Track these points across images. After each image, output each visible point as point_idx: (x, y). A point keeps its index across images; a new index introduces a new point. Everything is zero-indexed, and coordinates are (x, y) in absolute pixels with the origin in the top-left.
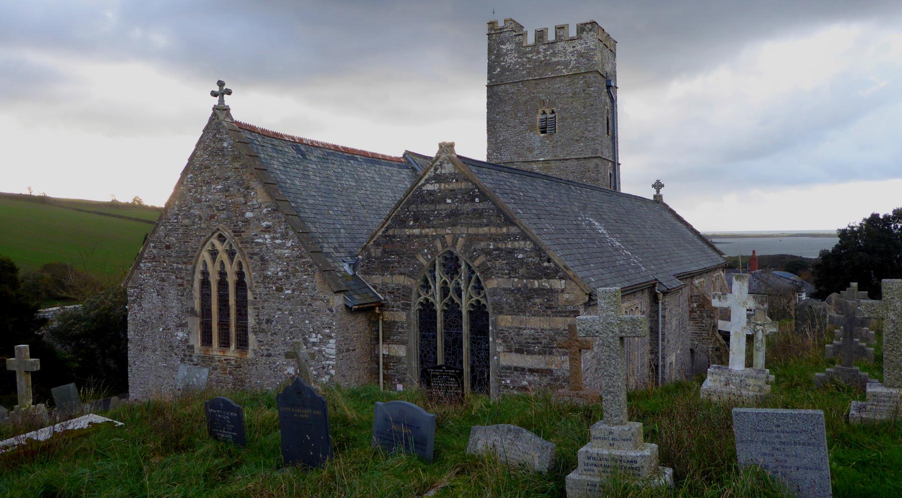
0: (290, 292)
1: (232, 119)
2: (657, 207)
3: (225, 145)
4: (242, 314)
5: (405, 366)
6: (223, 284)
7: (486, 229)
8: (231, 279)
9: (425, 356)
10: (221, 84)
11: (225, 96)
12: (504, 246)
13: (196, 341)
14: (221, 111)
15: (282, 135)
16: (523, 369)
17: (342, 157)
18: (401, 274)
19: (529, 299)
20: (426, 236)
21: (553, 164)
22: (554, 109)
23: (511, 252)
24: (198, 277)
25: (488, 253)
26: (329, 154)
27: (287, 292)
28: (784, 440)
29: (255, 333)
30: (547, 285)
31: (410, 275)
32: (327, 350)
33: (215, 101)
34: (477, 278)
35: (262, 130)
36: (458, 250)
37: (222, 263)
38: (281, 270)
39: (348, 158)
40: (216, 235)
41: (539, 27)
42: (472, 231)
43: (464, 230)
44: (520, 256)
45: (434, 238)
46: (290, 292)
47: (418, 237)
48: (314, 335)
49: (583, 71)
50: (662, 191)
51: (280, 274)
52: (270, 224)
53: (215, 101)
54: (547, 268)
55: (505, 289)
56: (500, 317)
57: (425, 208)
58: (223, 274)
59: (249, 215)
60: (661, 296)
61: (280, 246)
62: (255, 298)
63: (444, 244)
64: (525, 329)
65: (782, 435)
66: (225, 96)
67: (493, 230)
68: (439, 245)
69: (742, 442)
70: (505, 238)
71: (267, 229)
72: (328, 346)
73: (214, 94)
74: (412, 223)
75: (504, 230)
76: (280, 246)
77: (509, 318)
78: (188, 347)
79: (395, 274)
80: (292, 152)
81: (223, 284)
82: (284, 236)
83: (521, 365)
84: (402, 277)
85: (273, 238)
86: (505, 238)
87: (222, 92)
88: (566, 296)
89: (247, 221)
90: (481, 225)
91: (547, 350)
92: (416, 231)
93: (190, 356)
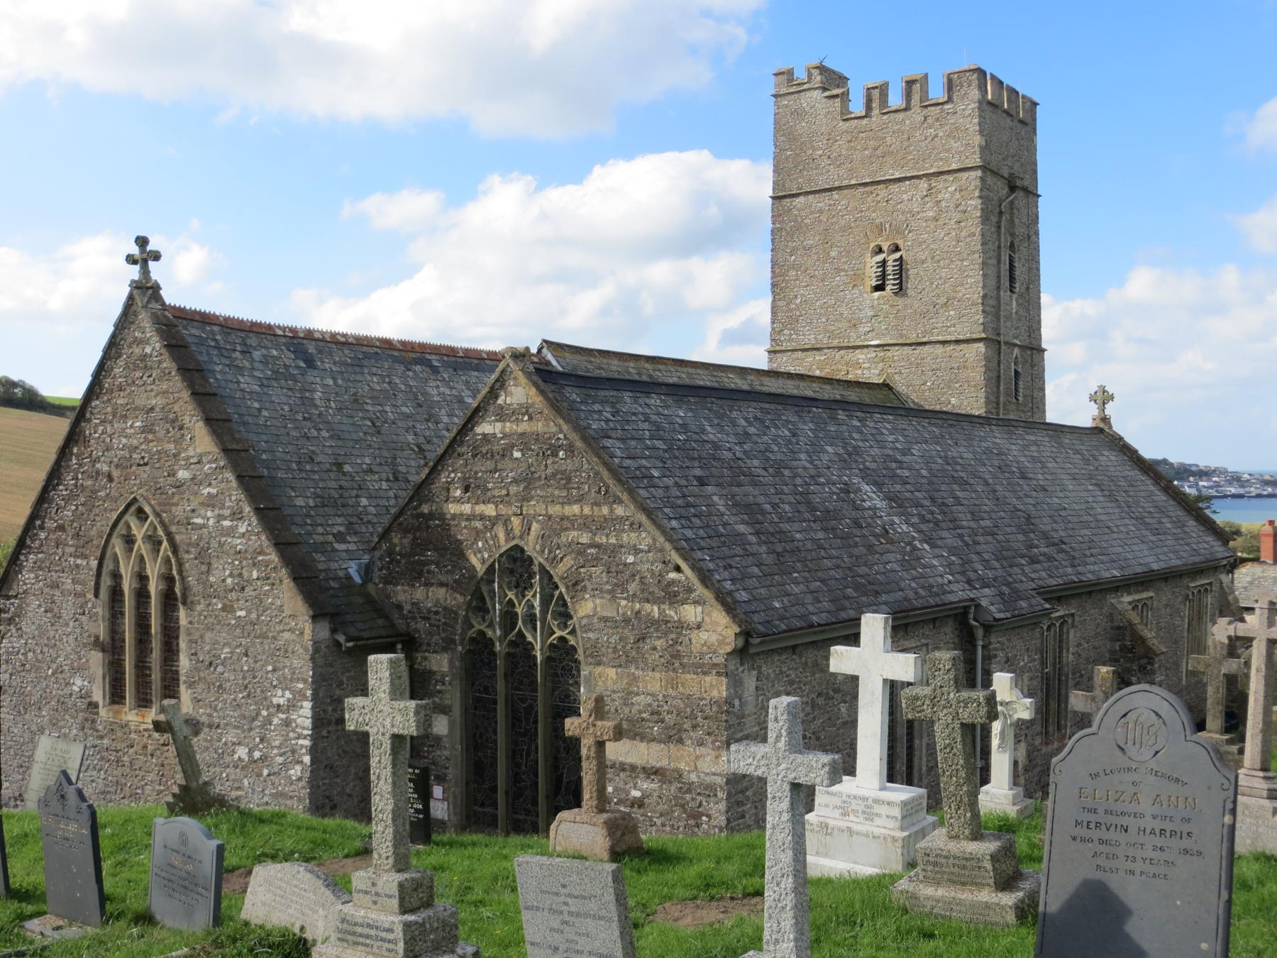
0: (243, 613)
1: (163, 304)
2: (1015, 448)
3: (148, 350)
4: (170, 651)
5: (446, 753)
6: (142, 595)
7: (576, 509)
8: (154, 587)
9: (481, 737)
10: (142, 242)
11: (151, 264)
12: (604, 540)
13: (98, 696)
14: (146, 290)
15: (269, 327)
16: (633, 768)
17: (396, 360)
18: (441, 584)
19: (642, 639)
20: (482, 517)
21: (895, 352)
22: (900, 242)
23: (615, 550)
24: (106, 581)
25: (580, 550)
26: (367, 356)
27: (239, 613)
28: (573, 909)
29: (191, 685)
30: (672, 613)
31: (456, 587)
32: (299, 721)
33: (134, 272)
34: (561, 596)
35: (227, 319)
36: (531, 546)
37: (142, 559)
38: (231, 575)
39: (408, 364)
40: (133, 509)
41: (914, 72)
42: (555, 510)
43: (541, 509)
44: (631, 559)
45: (494, 521)
46: (243, 613)
47: (470, 518)
48: (280, 693)
49: (954, 166)
50: (1110, 409)
51: (229, 581)
52: (214, 491)
53: (134, 272)
54: (673, 582)
55: (605, 619)
56: (599, 669)
57: (481, 466)
58: (142, 578)
59: (183, 474)
60: (980, 633)
61: (231, 532)
62: (191, 623)
63: (509, 533)
64: (637, 694)
65: (569, 900)
66: (151, 264)
67: (587, 510)
68: (502, 536)
69: (527, 908)
70: (603, 525)
71: (211, 502)
72: (301, 712)
73: (131, 260)
74: (458, 493)
75: (605, 510)
76: (231, 532)
77: (611, 672)
78: (90, 704)
79: (432, 585)
80: (288, 358)
81: (142, 595)
82: (237, 515)
83: (630, 760)
84: (443, 590)
85: (220, 518)
86: (603, 525)
87: (144, 255)
88: (704, 636)
89: (179, 486)
90: (569, 501)
91: (674, 736)
92: (467, 508)
93: (94, 721)
